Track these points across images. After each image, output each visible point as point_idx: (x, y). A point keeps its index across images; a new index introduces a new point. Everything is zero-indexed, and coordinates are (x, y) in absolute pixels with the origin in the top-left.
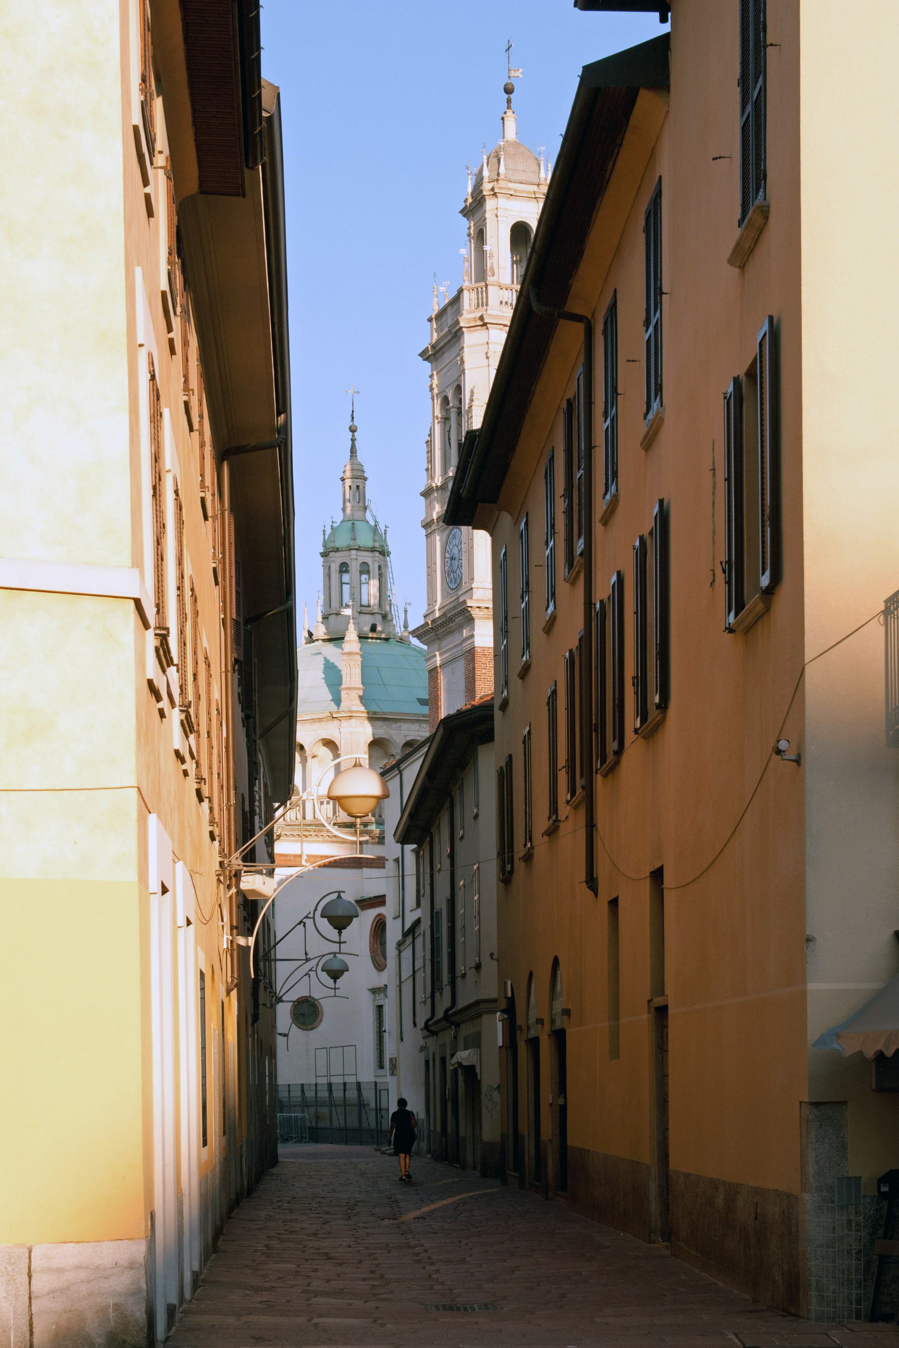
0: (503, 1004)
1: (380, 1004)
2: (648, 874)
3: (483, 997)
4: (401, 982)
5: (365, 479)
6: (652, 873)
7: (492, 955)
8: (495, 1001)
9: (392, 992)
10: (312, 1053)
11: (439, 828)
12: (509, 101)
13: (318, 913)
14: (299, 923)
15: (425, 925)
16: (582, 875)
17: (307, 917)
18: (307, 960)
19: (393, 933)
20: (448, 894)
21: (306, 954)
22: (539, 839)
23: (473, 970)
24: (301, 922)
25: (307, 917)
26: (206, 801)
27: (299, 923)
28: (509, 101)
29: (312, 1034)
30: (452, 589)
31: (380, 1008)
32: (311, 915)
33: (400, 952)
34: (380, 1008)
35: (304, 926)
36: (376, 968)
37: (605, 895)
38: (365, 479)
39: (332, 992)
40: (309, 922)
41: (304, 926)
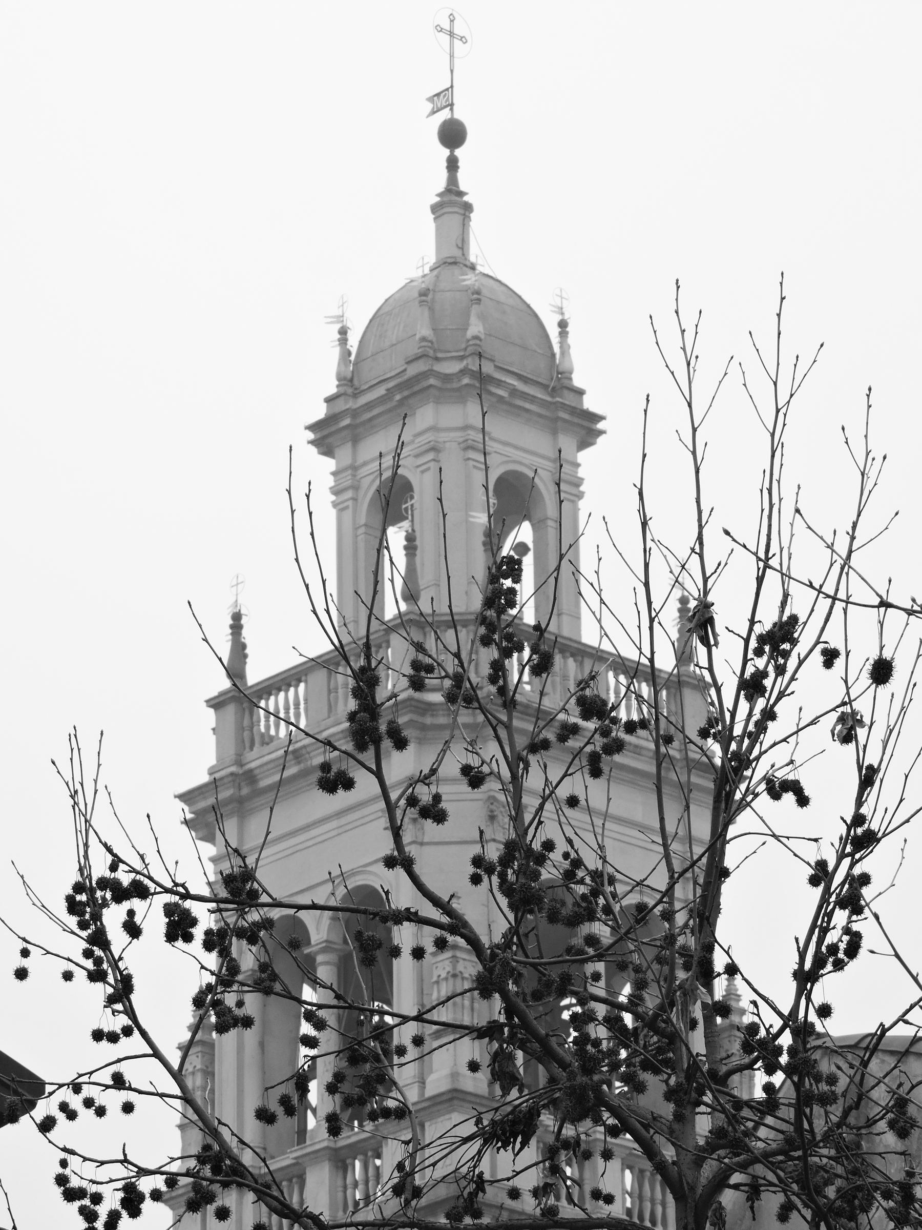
28: (452, 165)
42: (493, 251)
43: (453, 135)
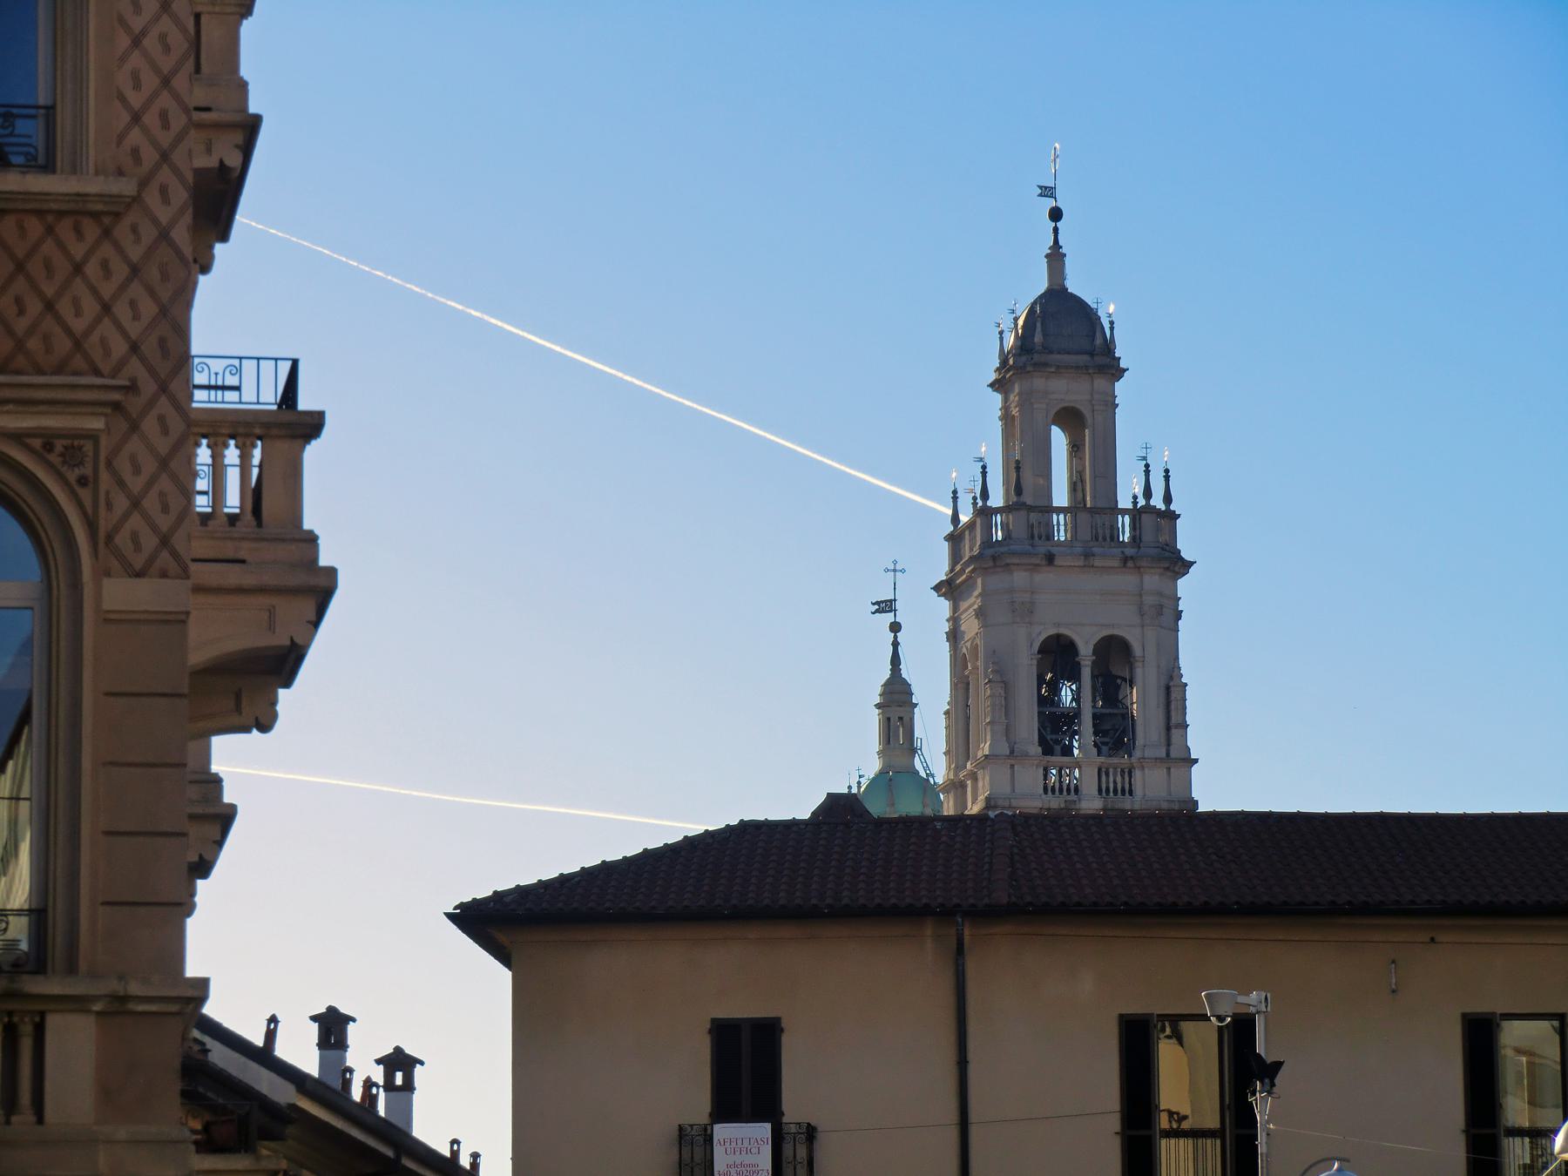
28: (1056, 230)
42: (1073, 286)
43: (1056, 214)
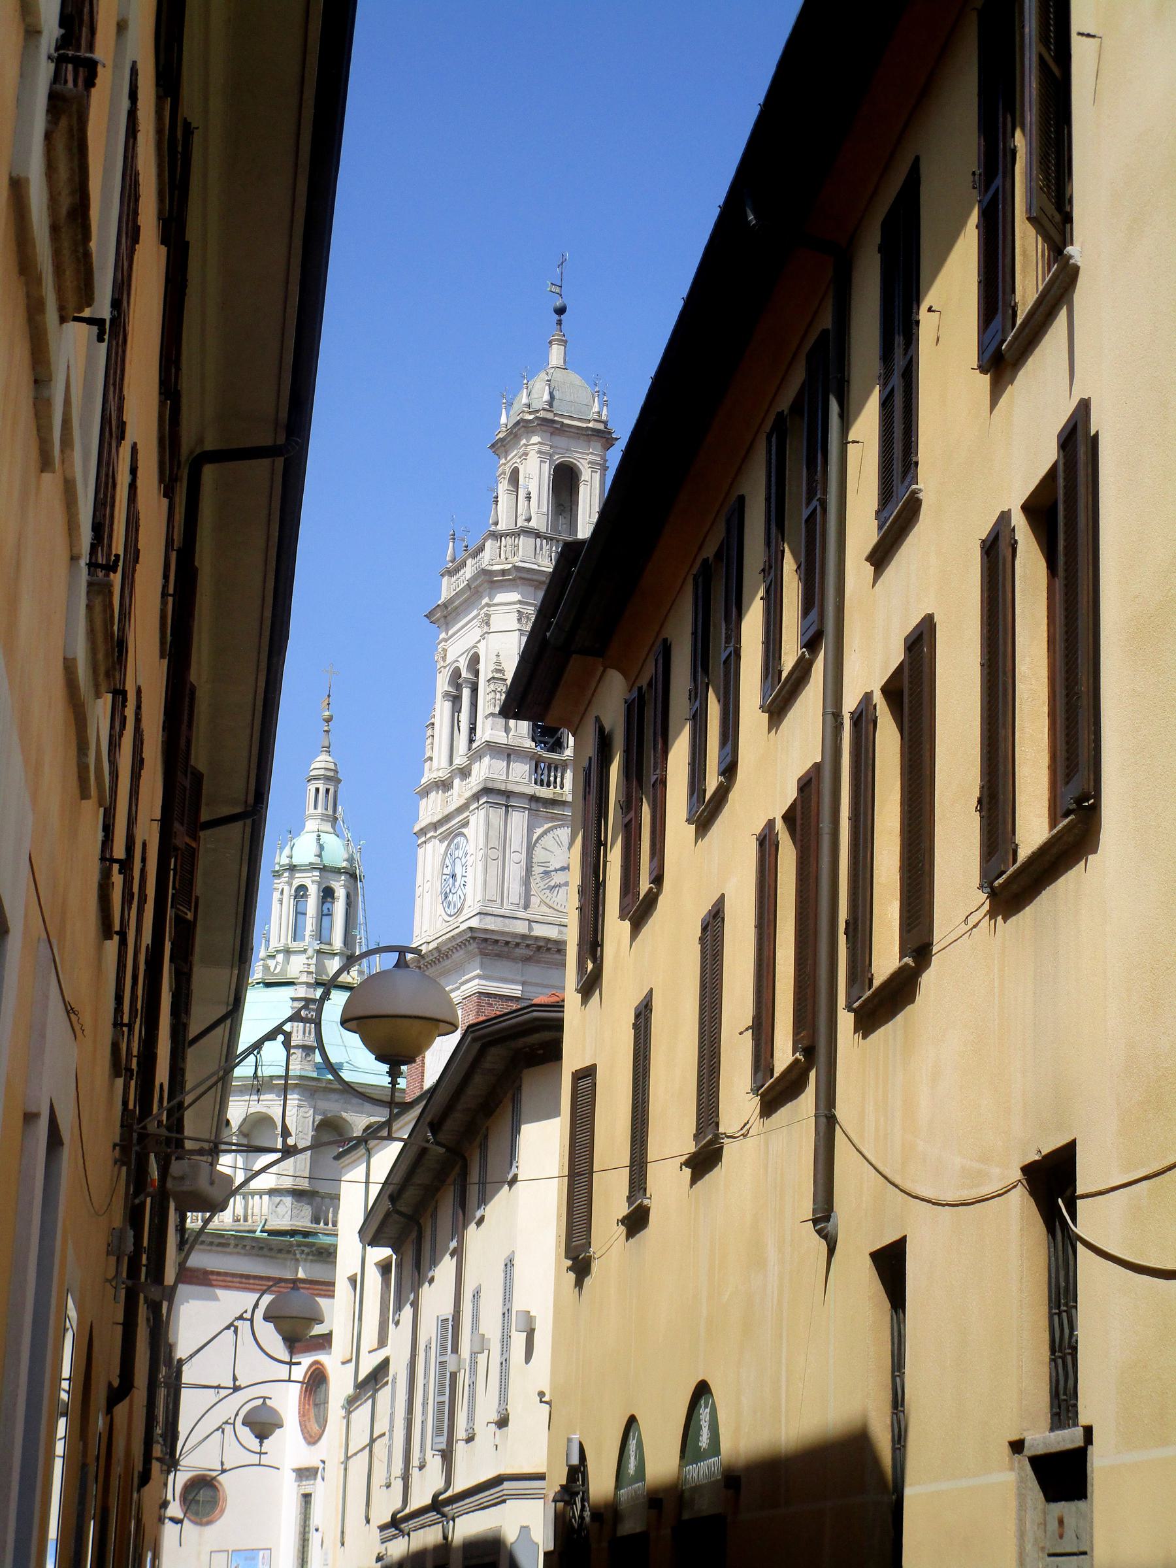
0: (559, 1477)
1: (307, 1491)
2: (1018, 1175)
3: (509, 1471)
4: (348, 1458)
5: (339, 781)
6: (1027, 1170)
7: (541, 1394)
8: (541, 1477)
9: (333, 1472)
10: (205, 1558)
11: (434, 1215)
12: (559, 323)
13: (260, 1313)
14: (228, 1328)
15: (399, 1369)
16: (807, 1208)
17: (241, 1318)
18: (236, 1389)
19: (340, 1384)
20: (448, 1311)
21: (235, 1379)
22: (667, 1178)
23: (493, 1427)
24: (231, 1325)
25: (241, 1318)
26: (116, 938)
27: (228, 1328)
28: (559, 323)
29: (209, 1531)
30: (450, 916)
31: (307, 1497)
32: (247, 1316)
33: (349, 1413)
34: (307, 1497)
35: (236, 1332)
36: (305, 1438)
37: (859, 1239)
38: (339, 781)
39: (255, 1459)
40: (244, 1326)
41: (236, 1332)
